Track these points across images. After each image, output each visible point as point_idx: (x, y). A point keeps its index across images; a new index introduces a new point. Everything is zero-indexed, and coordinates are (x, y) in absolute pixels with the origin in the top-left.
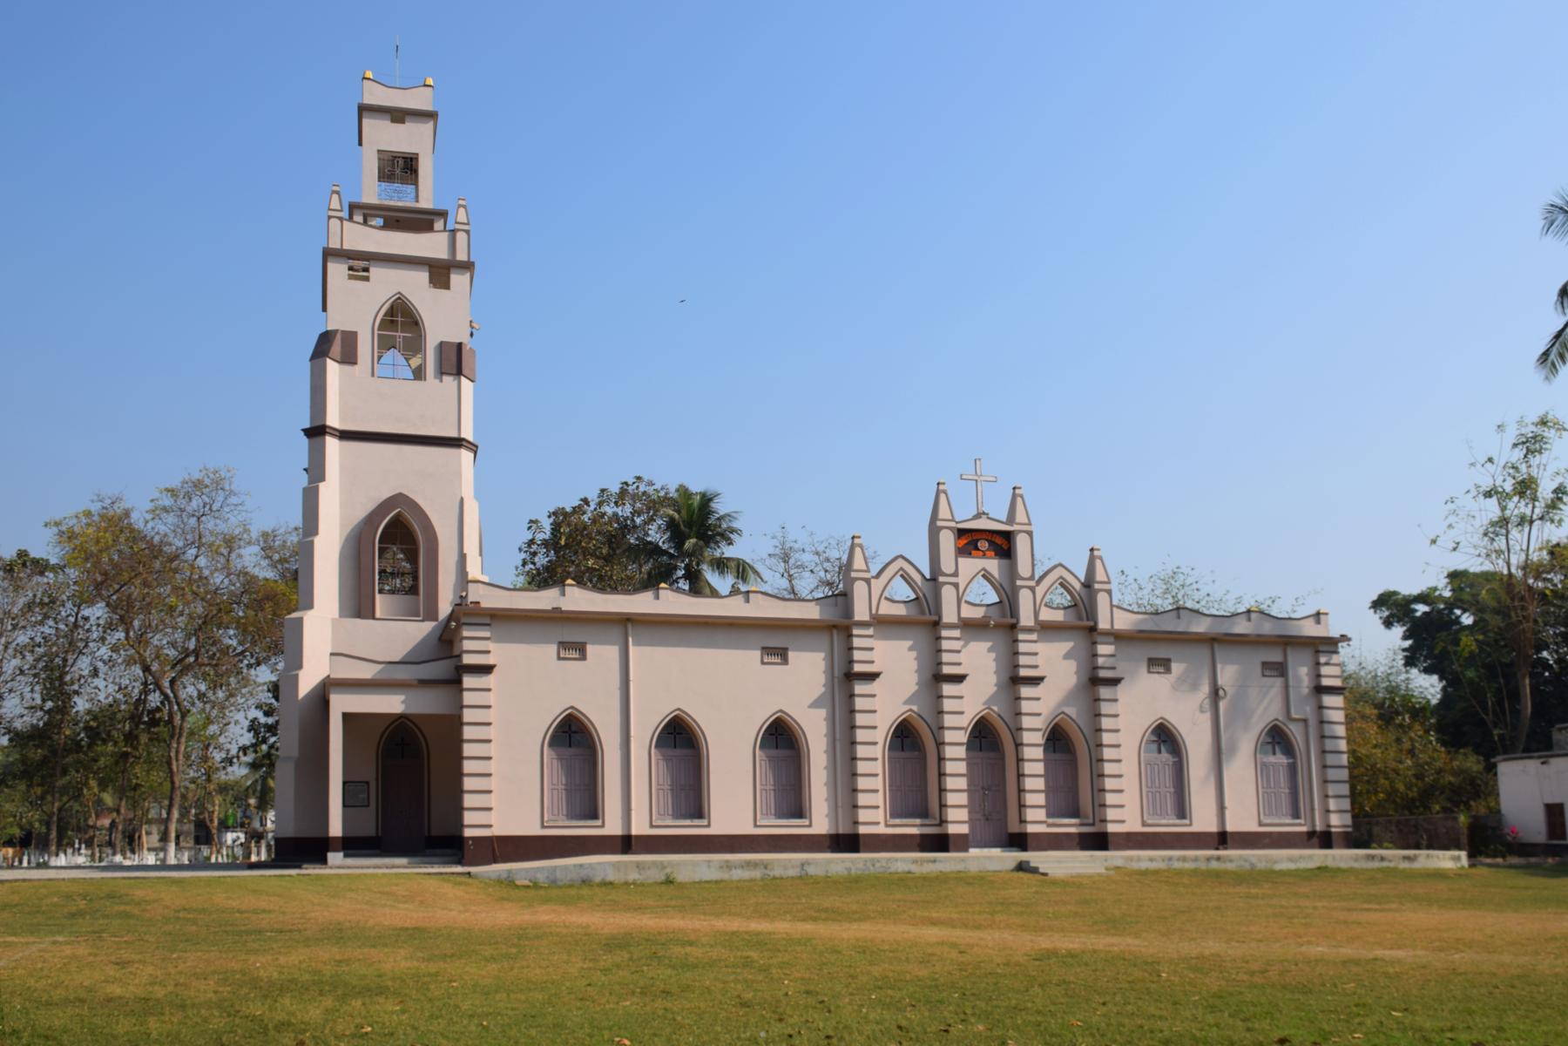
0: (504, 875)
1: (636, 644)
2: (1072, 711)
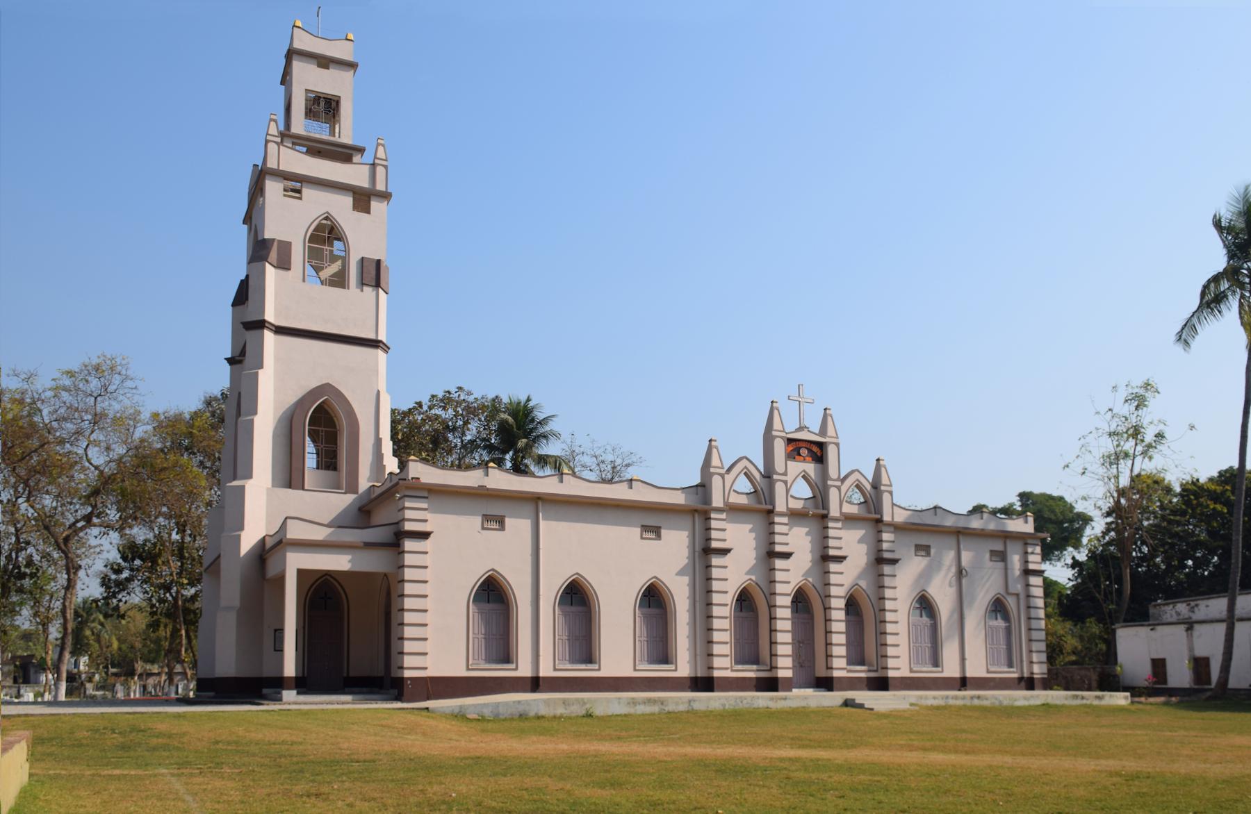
0: (456, 711)
1: (543, 519)
2: (863, 584)
